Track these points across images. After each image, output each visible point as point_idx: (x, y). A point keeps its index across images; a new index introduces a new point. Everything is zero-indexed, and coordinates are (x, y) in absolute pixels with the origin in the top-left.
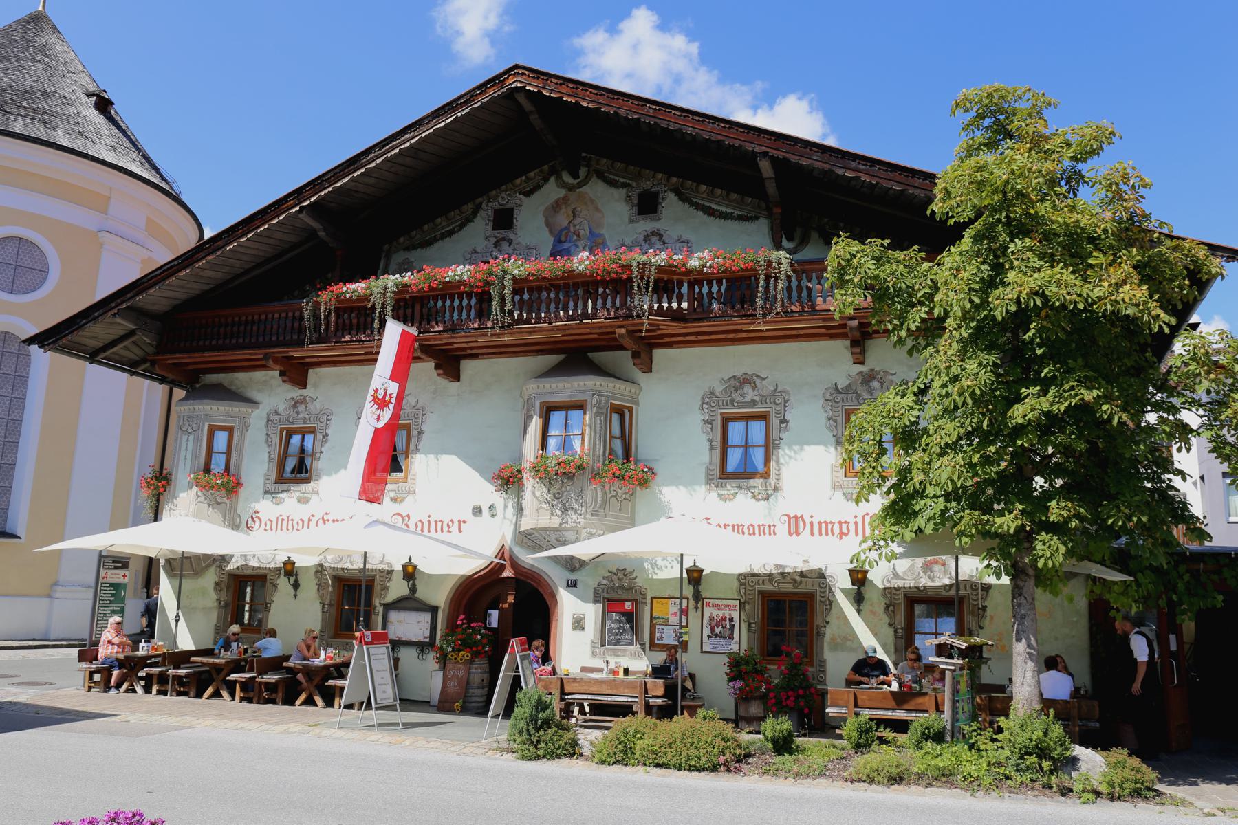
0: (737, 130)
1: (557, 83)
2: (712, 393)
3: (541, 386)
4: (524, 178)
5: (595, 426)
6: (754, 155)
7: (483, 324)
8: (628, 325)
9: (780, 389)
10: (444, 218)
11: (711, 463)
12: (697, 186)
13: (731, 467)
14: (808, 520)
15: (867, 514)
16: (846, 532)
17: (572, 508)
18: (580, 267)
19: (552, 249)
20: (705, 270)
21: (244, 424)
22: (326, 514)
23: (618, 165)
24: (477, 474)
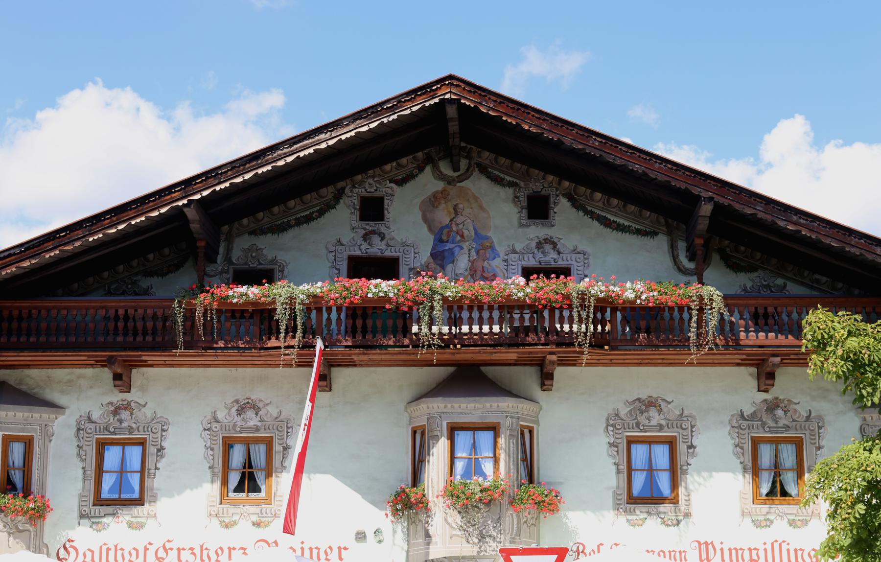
0: (684, 173)
1: (495, 101)
2: (617, 415)
3: (430, 406)
4: (394, 164)
5: (509, 450)
6: (698, 198)
7: (399, 342)
8: (559, 352)
9: (686, 413)
10: (298, 200)
11: (618, 487)
12: (591, 194)
13: (636, 490)
14: (718, 547)
15: (776, 541)
16: (756, 559)
17: (490, 536)
18: (519, 294)
19: (433, 248)
20: (639, 301)
21: (46, 433)
22: (169, 541)
23: (502, 160)
24: (359, 496)
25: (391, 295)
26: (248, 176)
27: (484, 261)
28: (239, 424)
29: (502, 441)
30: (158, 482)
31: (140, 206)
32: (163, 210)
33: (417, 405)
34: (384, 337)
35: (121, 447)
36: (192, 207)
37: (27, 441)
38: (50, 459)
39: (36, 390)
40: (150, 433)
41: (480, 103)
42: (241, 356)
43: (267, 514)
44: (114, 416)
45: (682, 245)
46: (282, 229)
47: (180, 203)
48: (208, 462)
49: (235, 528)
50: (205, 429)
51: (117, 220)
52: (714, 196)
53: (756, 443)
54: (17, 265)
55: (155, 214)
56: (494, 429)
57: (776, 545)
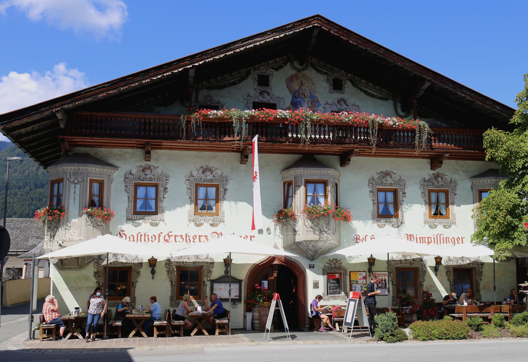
1: (338, 29)
2: (373, 179)
4: (274, 61)
8: (360, 148)
9: (402, 178)
11: (374, 210)
14: (415, 237)
15: (438, 234)
17: (324, 231)
19: (292, 100)
20: (394, 126)
21: (110, 179)
22: (170, 232)
25: (288, 117)
26: (222, 56)
27: (315, 107)
28: (203, 178)
29: (329, 188)
30: (164, 204)
31: (168, 67)
32: (180, 70)
33: (288, 171)
34: (281, 138)
35: (145, 188)
36: (194, 69)
37: (101, 182)
38: (112, 192)
39: (104, 158)
40: (160, 181)
41: (331, 29)
42: (211, 144)
43: (217, 220)
44: (143, 172)
45: (399, 105)
46: (221, 87)
47: (189, 67)
48: (189, 195)
49: (202, 227)
50: (187, 180)
51: (157, 73)
52: (432, 79)
53: (430, 191)
54: (106, 92)
55: (176, 71)
56: (325, 183)
57: (438, 236)
